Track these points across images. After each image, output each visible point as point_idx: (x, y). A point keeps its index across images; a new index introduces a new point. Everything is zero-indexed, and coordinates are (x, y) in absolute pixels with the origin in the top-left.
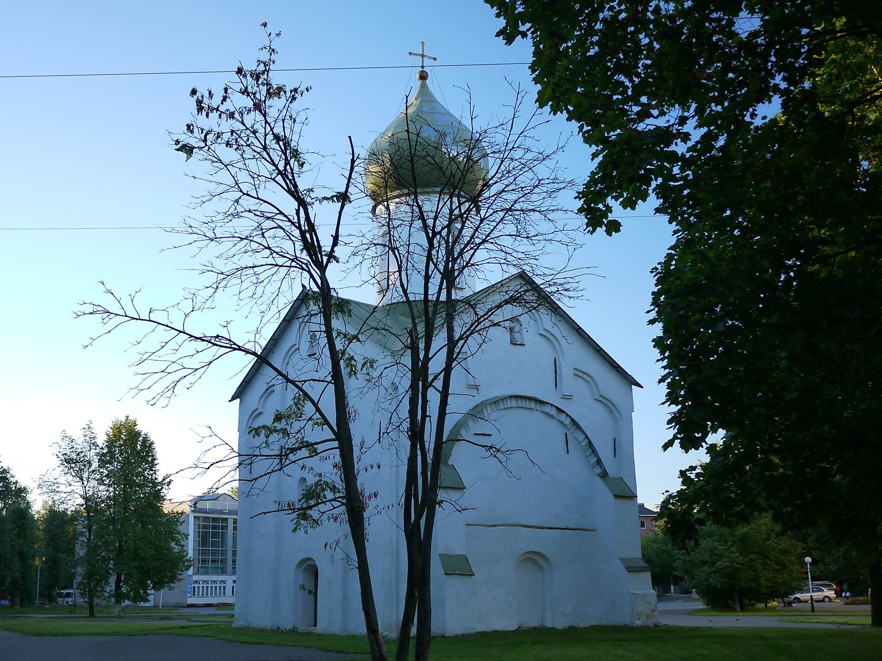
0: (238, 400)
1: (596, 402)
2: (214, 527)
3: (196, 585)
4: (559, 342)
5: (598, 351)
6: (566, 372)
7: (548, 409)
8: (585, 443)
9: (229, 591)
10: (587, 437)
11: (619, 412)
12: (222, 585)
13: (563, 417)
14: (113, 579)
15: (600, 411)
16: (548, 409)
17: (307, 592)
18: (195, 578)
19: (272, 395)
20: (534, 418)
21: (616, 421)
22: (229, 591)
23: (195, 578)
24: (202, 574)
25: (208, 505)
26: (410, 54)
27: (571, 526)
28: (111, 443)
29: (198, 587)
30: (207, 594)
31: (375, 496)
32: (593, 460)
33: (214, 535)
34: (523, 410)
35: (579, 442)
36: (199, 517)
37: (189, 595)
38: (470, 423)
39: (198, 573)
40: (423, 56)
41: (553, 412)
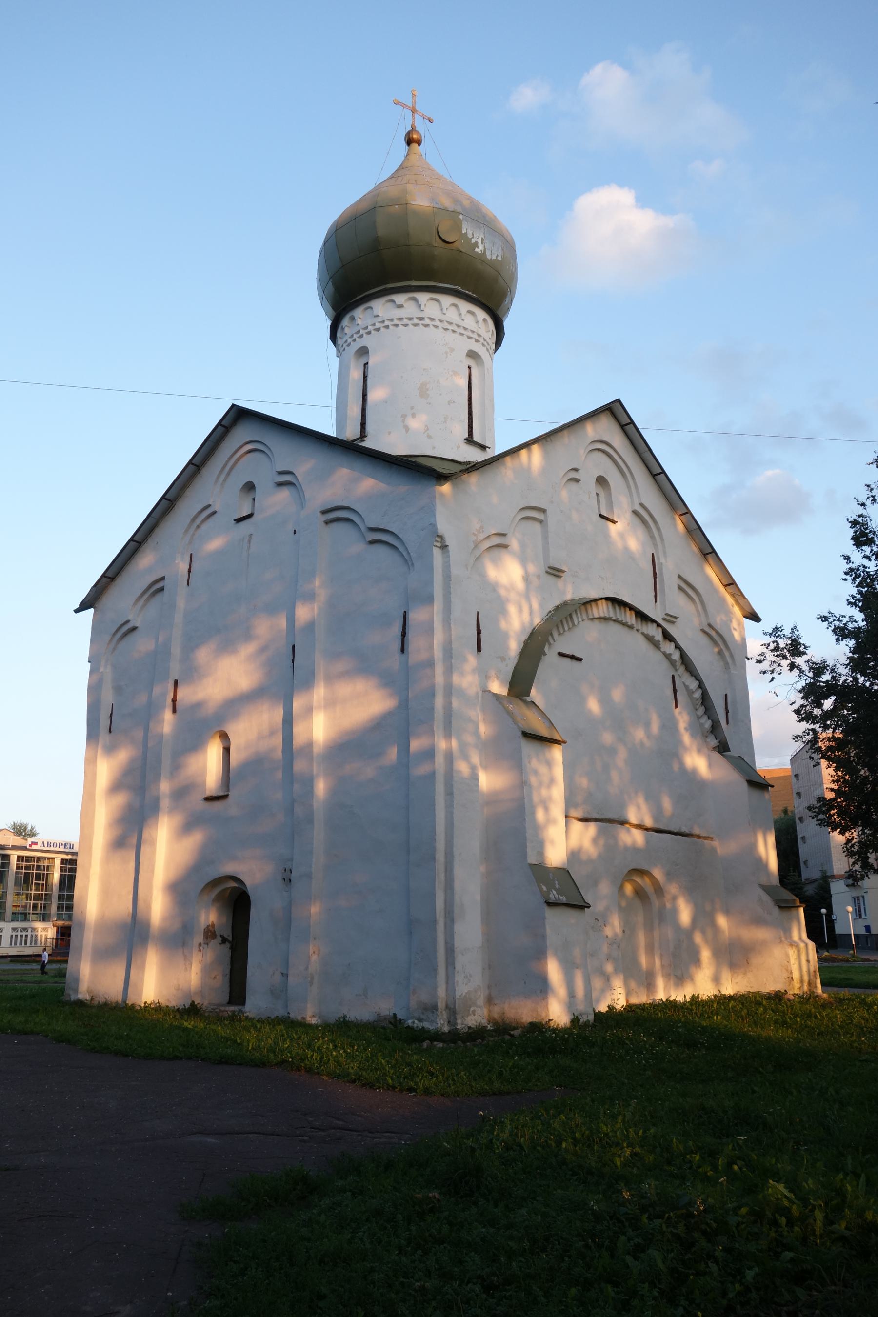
0: (92, 610)
1: (702, 635)
4: (659, 529)
5: (623, 427)
6: (670, 582)
8: (698, 694)
10: (701, 686)
11: (732, 656)
13: (669, 647)
17: (219, 939)
19: (159, 596)
20: (633, 642)
21: (727, 666)
26: (397, 103)
30: (16, 944)
31: (868, 486)
32: (708, 724)
33: (38, 877)
40: (414, 111)
41: (659, 636)
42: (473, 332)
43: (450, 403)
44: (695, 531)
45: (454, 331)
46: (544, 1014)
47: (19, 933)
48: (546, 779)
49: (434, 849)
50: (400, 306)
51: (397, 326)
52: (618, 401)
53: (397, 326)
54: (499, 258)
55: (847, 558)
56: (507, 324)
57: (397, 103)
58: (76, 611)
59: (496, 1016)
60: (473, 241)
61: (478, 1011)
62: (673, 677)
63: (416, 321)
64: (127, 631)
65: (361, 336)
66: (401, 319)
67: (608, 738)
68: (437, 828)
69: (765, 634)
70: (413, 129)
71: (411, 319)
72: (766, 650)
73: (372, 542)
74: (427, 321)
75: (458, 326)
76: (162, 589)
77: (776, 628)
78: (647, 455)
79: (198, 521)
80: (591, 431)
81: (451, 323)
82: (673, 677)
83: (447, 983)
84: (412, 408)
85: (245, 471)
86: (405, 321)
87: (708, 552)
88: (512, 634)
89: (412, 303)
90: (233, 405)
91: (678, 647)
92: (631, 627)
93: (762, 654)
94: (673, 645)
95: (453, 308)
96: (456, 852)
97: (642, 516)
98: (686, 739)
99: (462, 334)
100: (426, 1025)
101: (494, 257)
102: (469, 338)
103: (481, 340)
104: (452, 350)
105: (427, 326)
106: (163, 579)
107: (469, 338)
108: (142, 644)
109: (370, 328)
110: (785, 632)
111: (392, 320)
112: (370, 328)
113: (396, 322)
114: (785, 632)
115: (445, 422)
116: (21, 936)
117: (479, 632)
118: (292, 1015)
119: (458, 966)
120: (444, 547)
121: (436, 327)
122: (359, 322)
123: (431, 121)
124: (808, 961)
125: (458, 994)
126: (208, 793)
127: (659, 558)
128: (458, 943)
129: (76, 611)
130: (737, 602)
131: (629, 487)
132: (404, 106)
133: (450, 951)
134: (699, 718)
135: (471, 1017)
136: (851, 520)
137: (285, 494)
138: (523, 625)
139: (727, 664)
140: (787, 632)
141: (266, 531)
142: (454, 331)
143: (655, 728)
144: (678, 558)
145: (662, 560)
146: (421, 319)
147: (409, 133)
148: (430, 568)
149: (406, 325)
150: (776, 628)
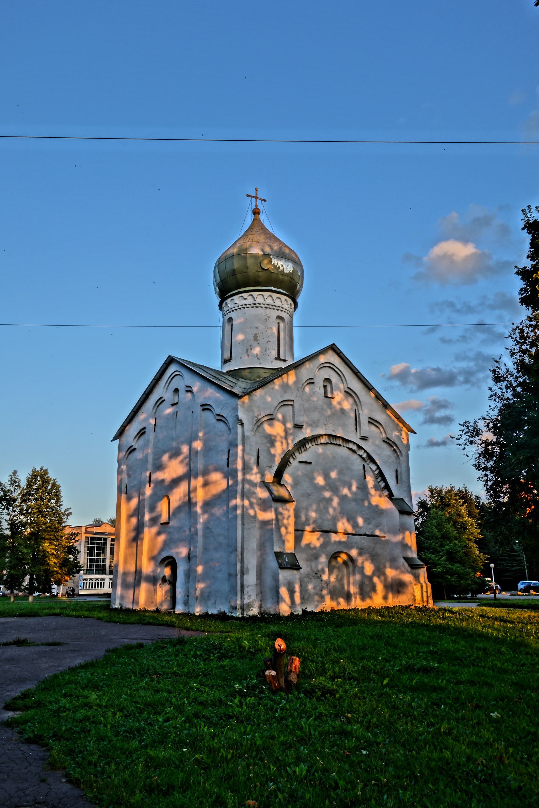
0: (118, 440)
2: (98, 544)
3: (85, 582)
4: (358, 398)
6: (364, 420)
7: (351, 446)
9: (107, 586)
12: (102, 582)
13: (361, 452)
14: (28, 577)
15: (387, 451)
16: (351, 446)
17: (168, 582)
18: (85, 577)
22: (107, 586)
23: (85, 577)
24: (89, 574)
25: (96, 530)
26: (248, 196)
27: (367, 533)
28: (30, 484)
29: (89, 585)
30: (92, 587)
33: (98, 549)
34: (334, 446)
35: (373, 471)
36: (88, 537)
37: (80, 588)
38: (297, 454)
39: (86, 574)
40: (256, 198)
41: (355, 448)
42: (279, 307)
43: (268, 342)
44: (378, 397)
45: (270, 308)
46: (278, 611)
47: (94, 582)
48: (286, 516)
49: (236, 546)
50: (246, 299)
51: (244, 308)
52: (334, 344)
53: (244, 308)
54: (291, 272)
55: (490, 389)
56: (299, 300)
57: (248, 196)
58: (112, 441)
59: (262, 612)
60: (277, 267)
61: (254, 609)
62: (364, 465)
63: (252, 305)
64: (131, 450)
65: (230, 312)
66: (246, 305)
67: (327, 494)
68: (238, 538)
69: (460, 425)
70: (257, 208)
71: (250, 304)
72: (461, 433)
73: (218, 420)
74: (258, 305)
75: (272, 305)
76: (144, 433)
77: (466, 422)
78: (351, 365)
79: (158, 404)
80: (322, 359)
81: (268, 305)
82: (364, 465)
83: (241, 598)
84: (251, 346)
85: (177, 383)
86: (248, 306)
87: (386, 406)
88: (277, 455)
89: (251, 297)
90: (169, 356)
91: (365, 451)
92: (340, 445)
93: (461, 435)
94: (363, 451)
95: (270, 297)
96: (245, 547)
97: (349, 393)
98: (372, 492)
99: (274, 309)
100: (233, 615)
101: (288, 272)
102: (278, 310)
103: (284, 310)
104: (269, 317)
105: (257, 307)
106: (145, 428)
107: (278, 310)
108: (138, 455)
109: (233, 309)
110: (471, 424)
111: (242, 305)
112: (233, 309)
113: (244, 306)
114: (471, 424)
115: (266, 351)
116: (90, 583)
117: (258, 457)
118: (190, 612)
119: (245, 592)
120: (242, 424)
121: (262, 307)
122: (229, 305)
123: (265, 201)
124: (427, 592)
125: (245, 603)
126: (162, 522)
127: (358, 411)
128: (245, 583)
129: (112, 441)
130: (404, 426)
131: (342, 380)
132: (252, 197)
133: (242, 586)
134: (379, 482)
135: (251, 612)
136: (492, 369)
137: (189, 394)
138: (284, 451)
139: (398, 455)
140: (472, 424)
141: (187, 409)
142: (270, 308)
143: (354, 488)
144: (369, 408)
145: (360, 412)
146: (255, 304)
147: (254, 209)
148: (237, 433)
149: (248, 308)
150: (466, 422)
